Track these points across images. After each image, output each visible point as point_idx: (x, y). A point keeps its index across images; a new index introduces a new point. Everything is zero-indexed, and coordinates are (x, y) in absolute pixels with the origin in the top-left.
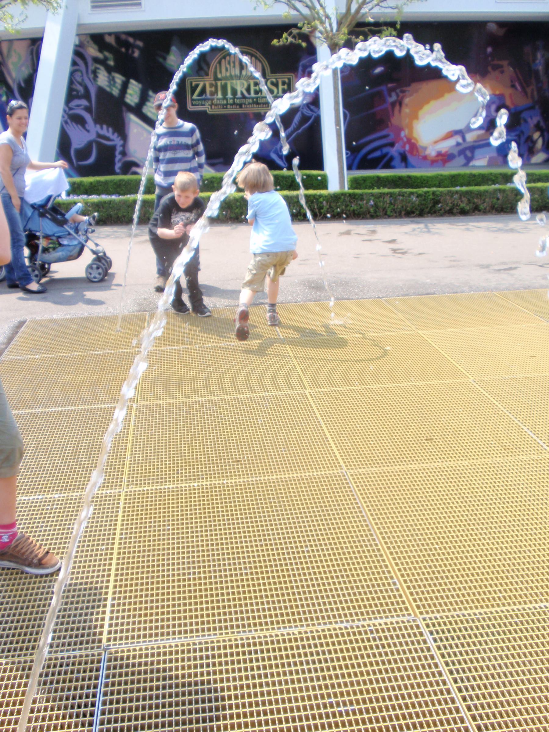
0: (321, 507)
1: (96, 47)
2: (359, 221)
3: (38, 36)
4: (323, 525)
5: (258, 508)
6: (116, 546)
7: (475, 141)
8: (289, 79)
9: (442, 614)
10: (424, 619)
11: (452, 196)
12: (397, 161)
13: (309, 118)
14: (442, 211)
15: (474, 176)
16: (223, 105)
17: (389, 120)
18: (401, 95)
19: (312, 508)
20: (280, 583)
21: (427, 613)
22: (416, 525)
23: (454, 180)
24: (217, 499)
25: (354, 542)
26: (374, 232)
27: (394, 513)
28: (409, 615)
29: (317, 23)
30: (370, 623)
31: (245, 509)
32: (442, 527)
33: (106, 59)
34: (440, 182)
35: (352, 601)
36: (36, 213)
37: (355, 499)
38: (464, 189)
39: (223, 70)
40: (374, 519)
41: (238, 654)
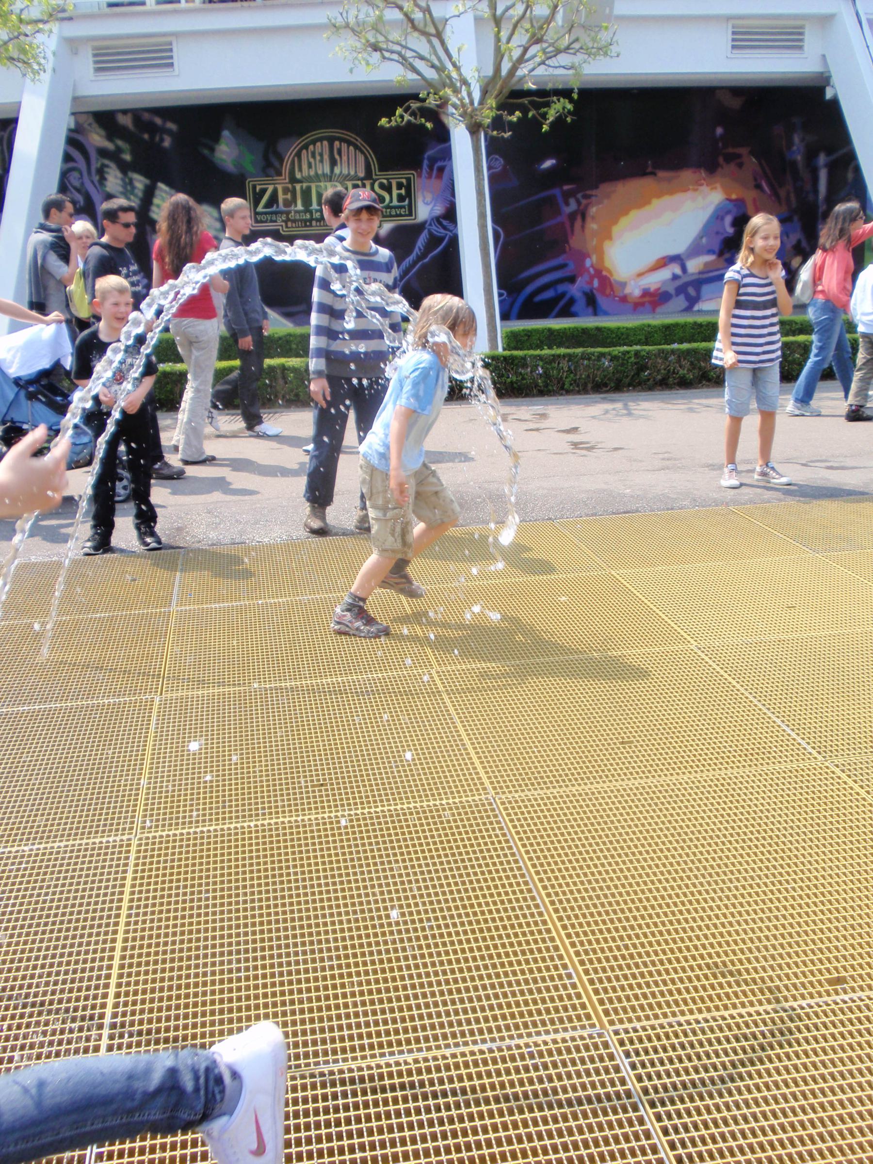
0: (453, 855)
1: (103, 132)
2: (520, 400)
3: (12, 115)
4: (456, 884)
5: (352, 860)
6: (121, 928)
7: (700, 273)
8: (408, 180)
9: (645, 1023)
10: (616, 1033)
11: (666, 359)
12: (580, 304)
13: (440, 240)
14: (651, 382)
15: (700, 325)
16: (306, 221)
17: (567, 242)
18: (584, 202)
19: (467, 853)
20: (385, 980)
21: (621, 1021)
22: (604, 880)
23: (669, 333)
24: (314, 844)
25: (506, 910)
26: (543, 416)
27: (570, 861)
28: (593, 1026)
29: (449, 91)
30: (530, 1041)
31: (331, 862)
32: (645, 883)
33: (119, 150)
34: (648, 335)
35: (552, 1000)
36: (23, 393)
37: (507, 841)
38: (685, 346)
39: (305, 167)
40: (538, 873)
41: (315, 1099)
